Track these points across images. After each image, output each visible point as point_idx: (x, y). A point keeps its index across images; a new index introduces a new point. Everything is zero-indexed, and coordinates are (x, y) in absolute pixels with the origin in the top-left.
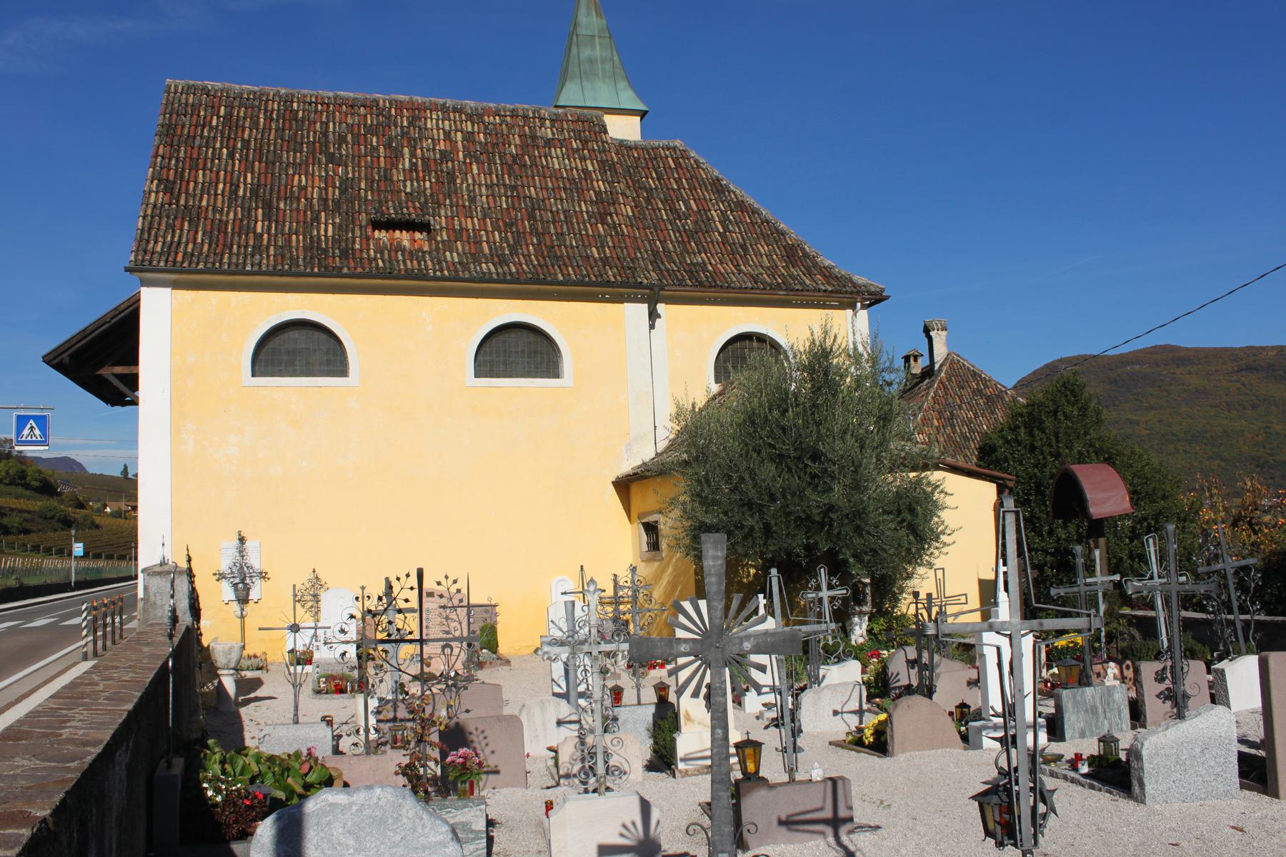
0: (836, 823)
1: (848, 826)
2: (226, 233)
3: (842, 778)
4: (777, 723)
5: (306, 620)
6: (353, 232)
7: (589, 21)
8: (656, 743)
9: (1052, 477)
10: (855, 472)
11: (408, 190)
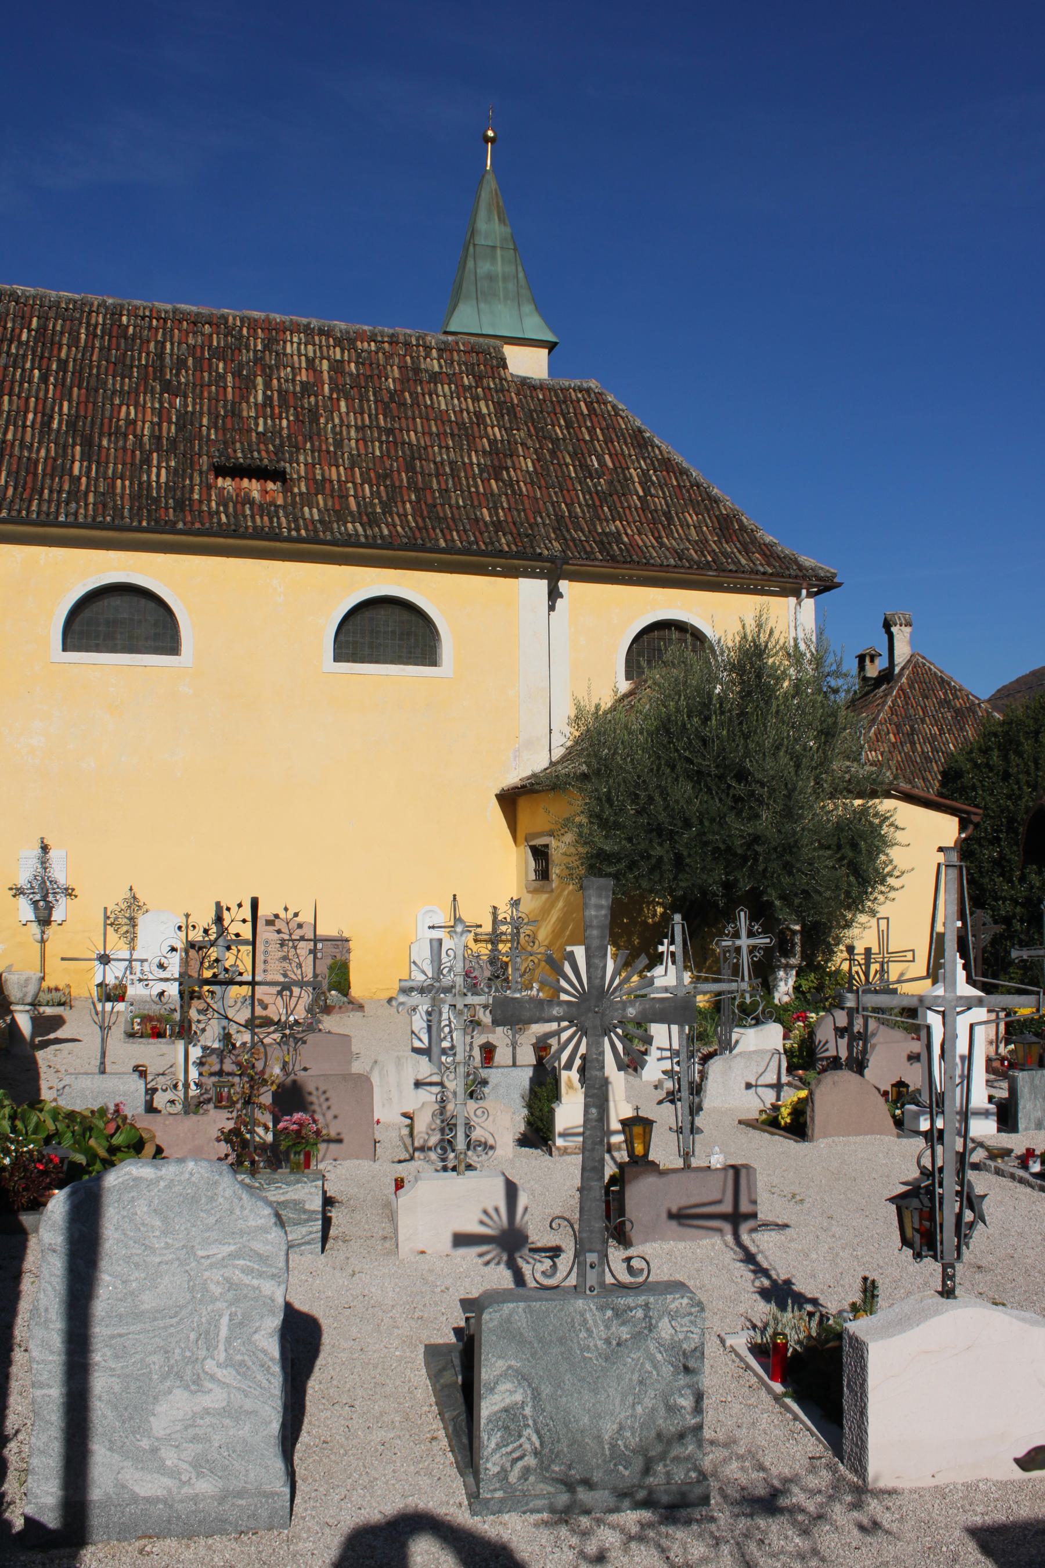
0: (736, 1218)
1: (751, 1224)
2: (35, 474)
3: (746, 1167)
4: (672, 1097)
5: (118, 948)
6: (191, 480)
7: (490, 228)
8: (532, 1114)
9: (1027, 810)
10: (789, 797)
11: (261, 429)
